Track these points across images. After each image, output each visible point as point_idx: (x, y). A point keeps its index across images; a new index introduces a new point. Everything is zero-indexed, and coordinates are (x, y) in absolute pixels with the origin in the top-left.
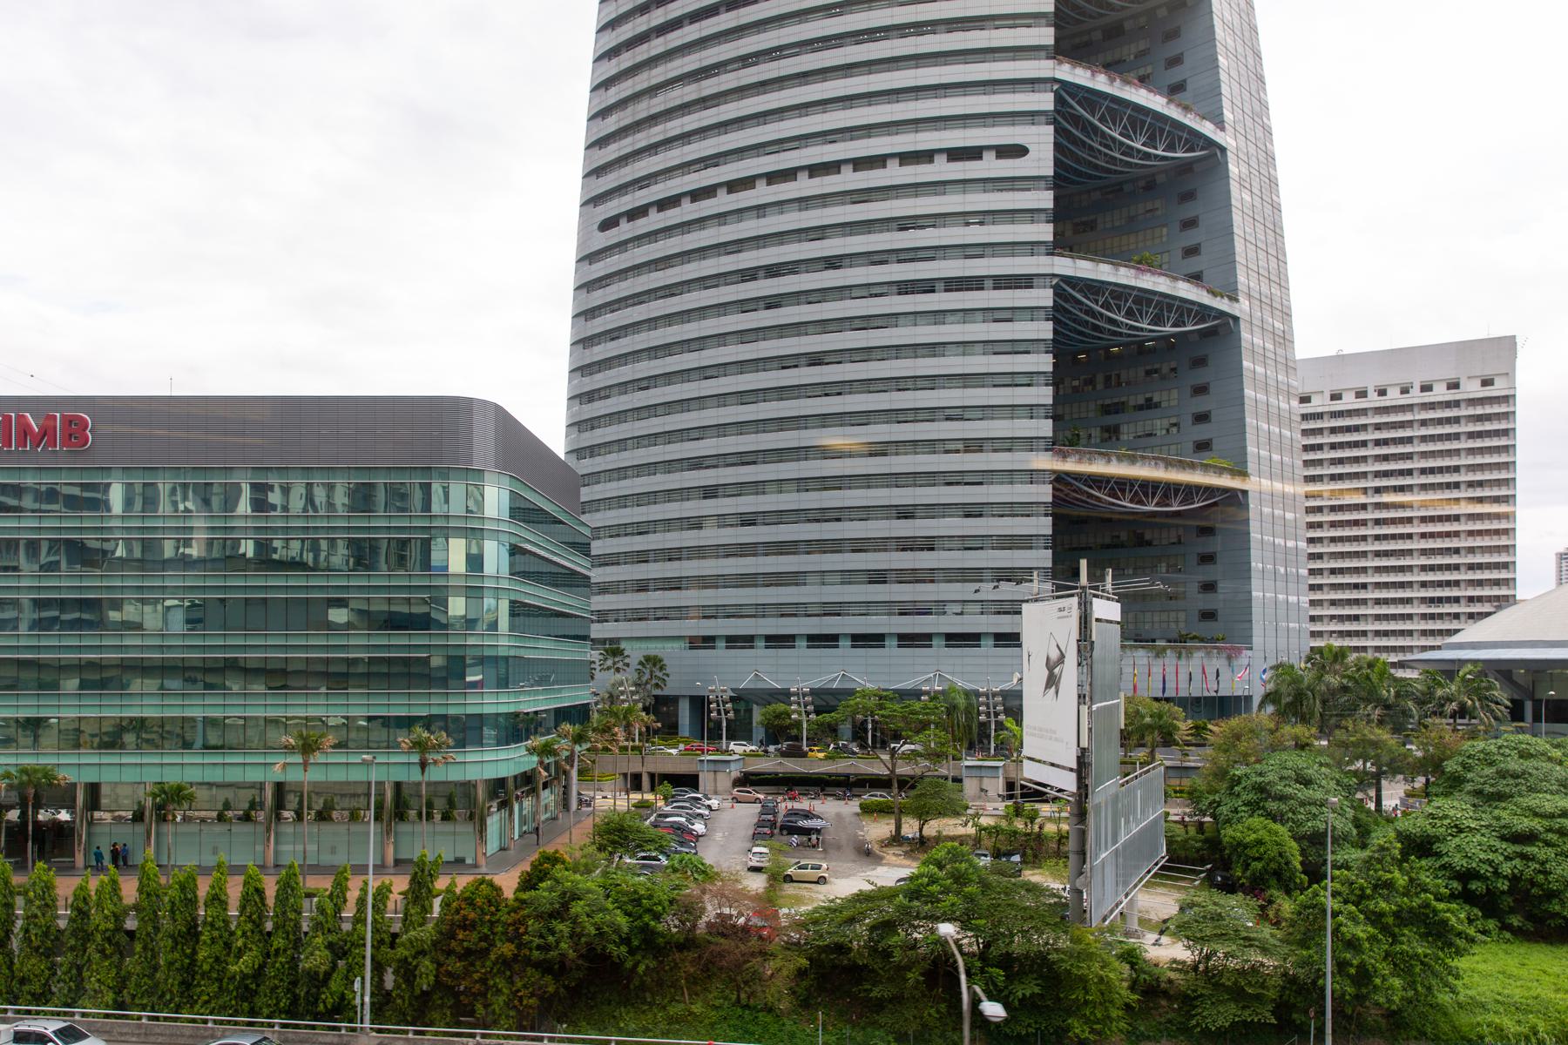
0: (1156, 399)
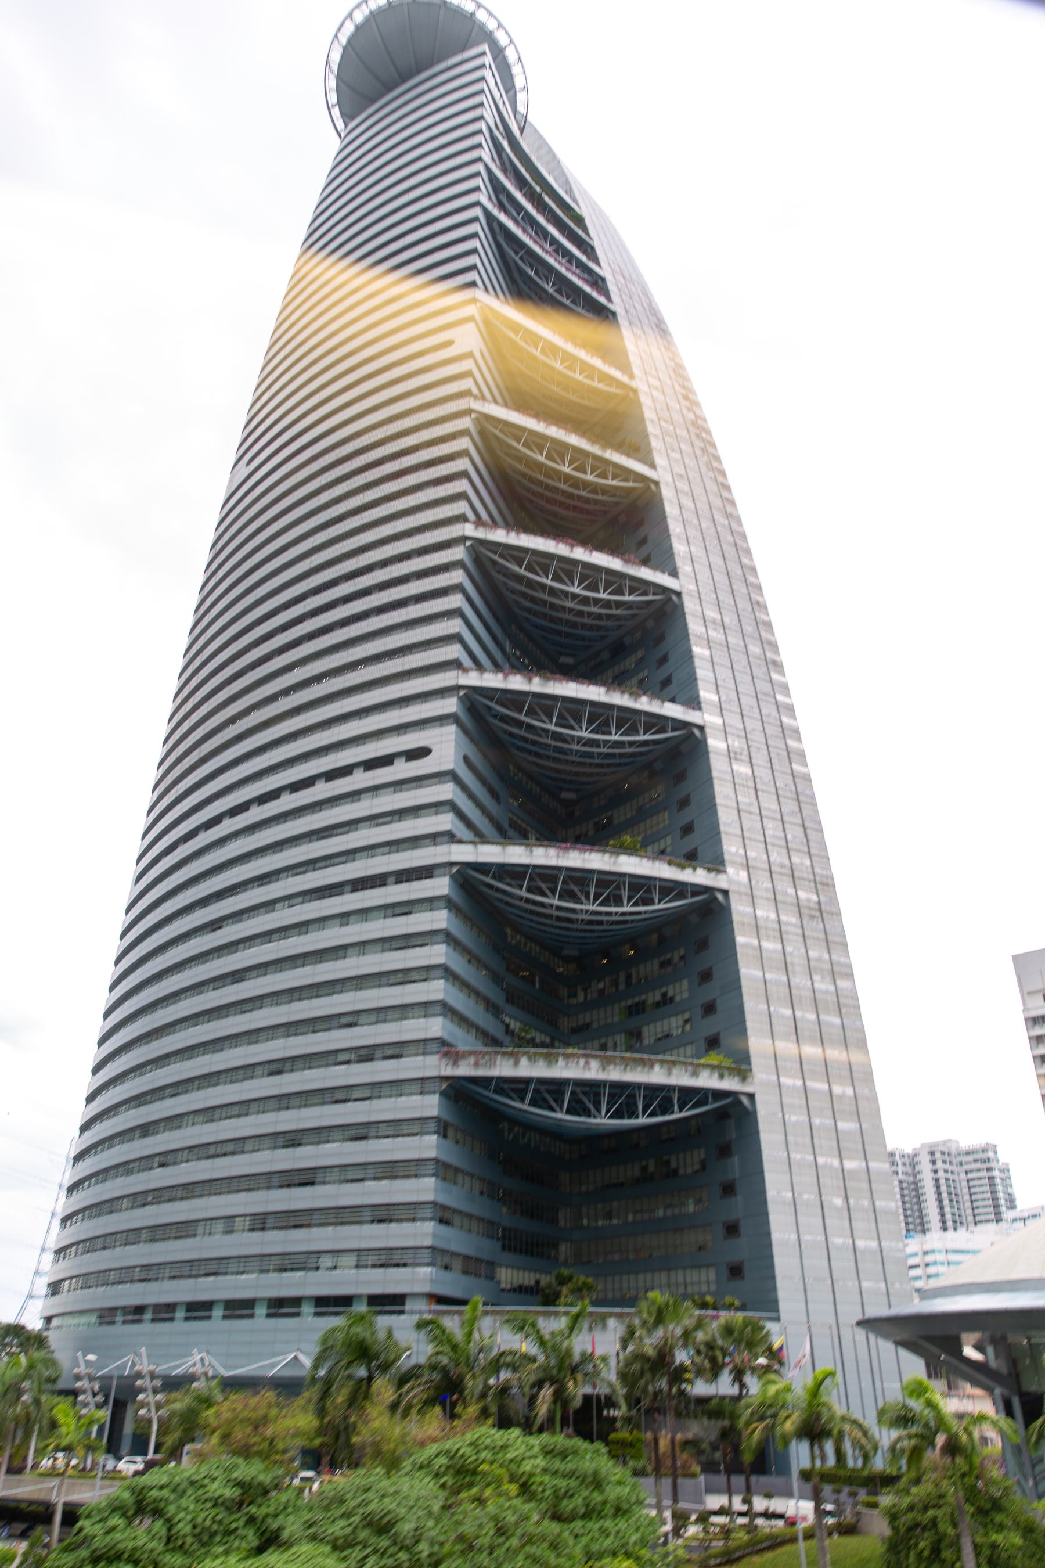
0: (670, 994)
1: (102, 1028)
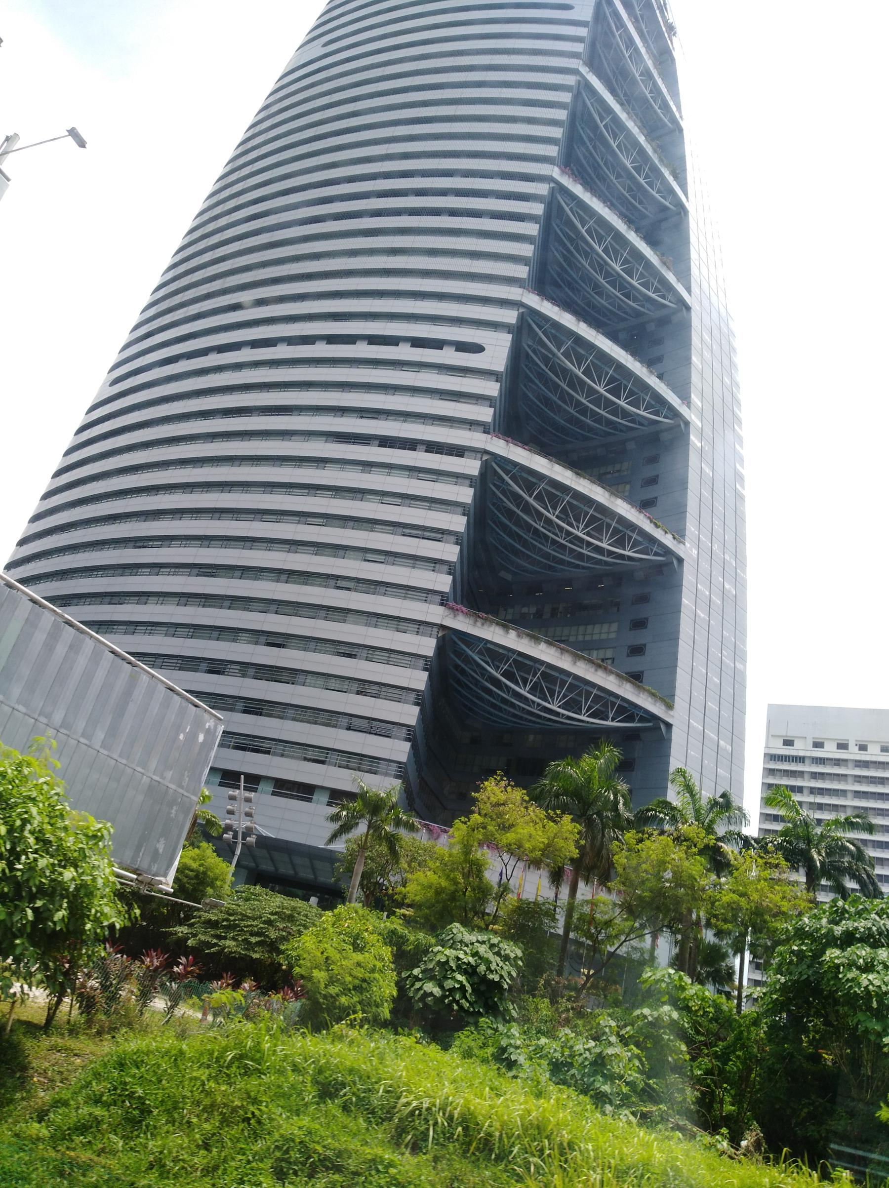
1: (50, 485)
